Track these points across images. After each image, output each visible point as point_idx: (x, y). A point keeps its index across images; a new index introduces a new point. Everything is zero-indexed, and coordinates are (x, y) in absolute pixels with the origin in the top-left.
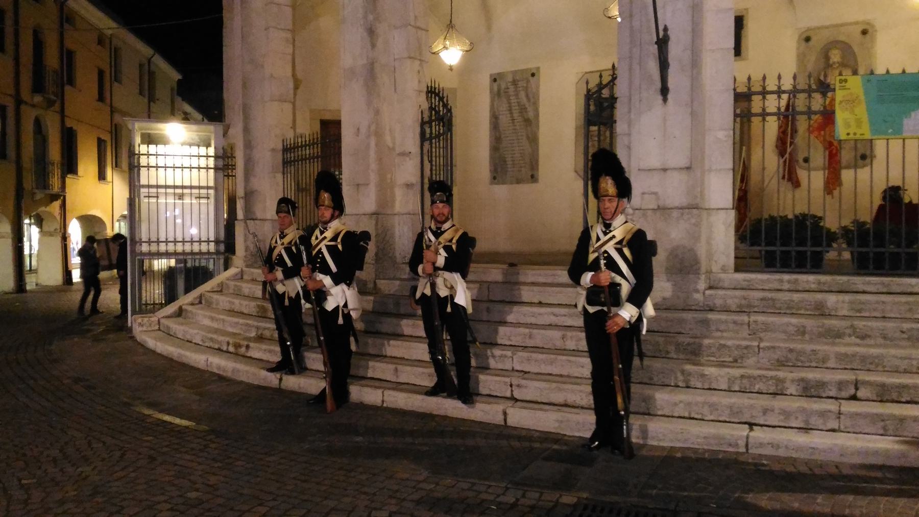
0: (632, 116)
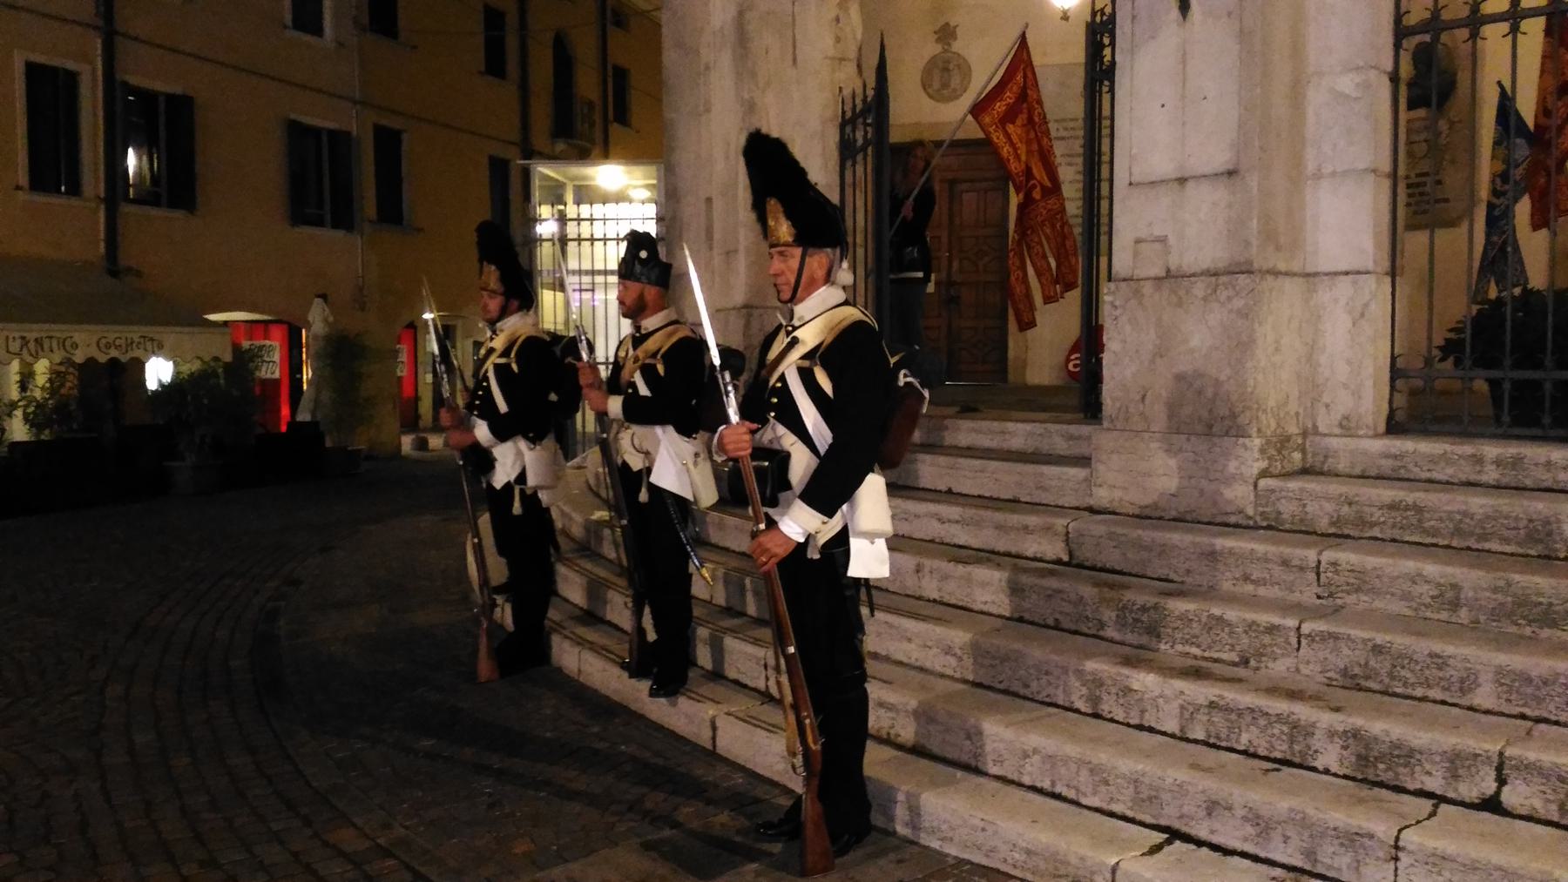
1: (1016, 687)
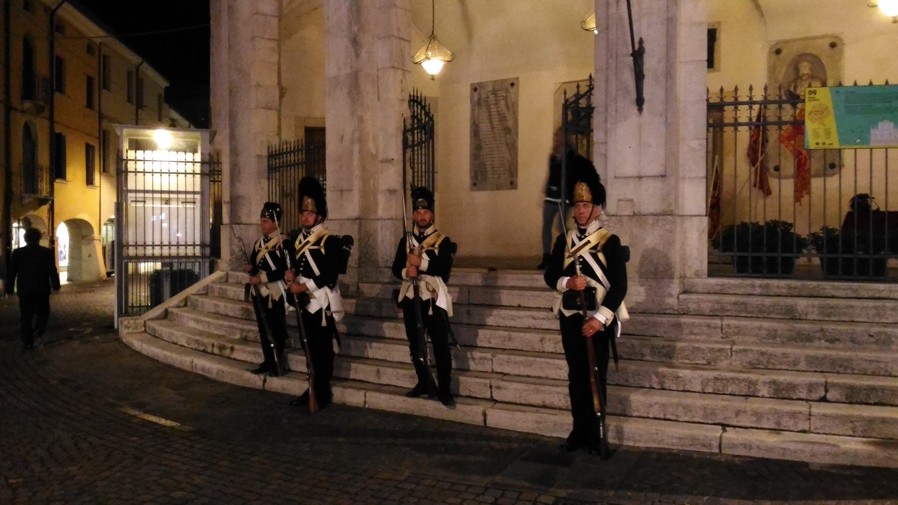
0: (609, 126)
1: (622, 382)
